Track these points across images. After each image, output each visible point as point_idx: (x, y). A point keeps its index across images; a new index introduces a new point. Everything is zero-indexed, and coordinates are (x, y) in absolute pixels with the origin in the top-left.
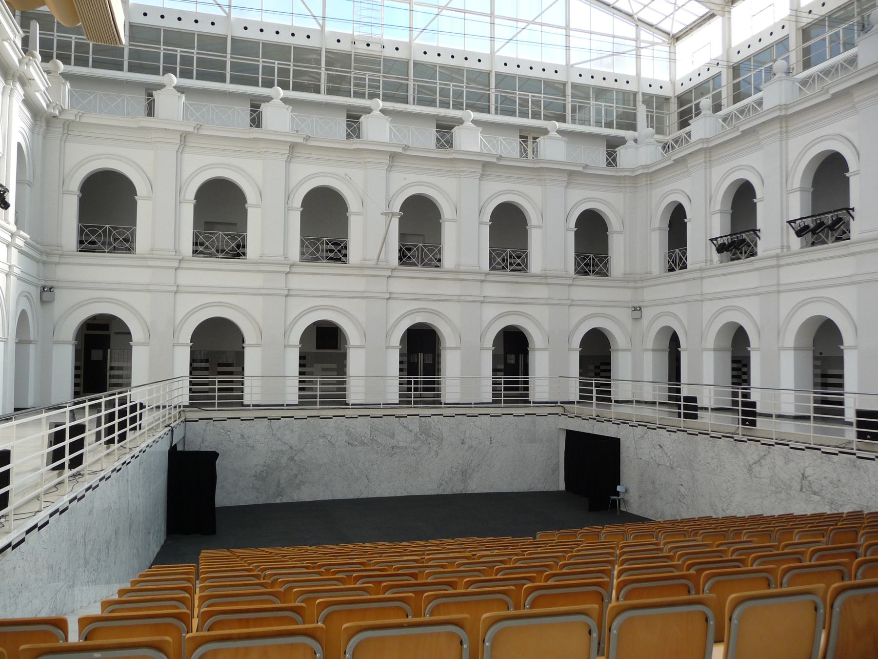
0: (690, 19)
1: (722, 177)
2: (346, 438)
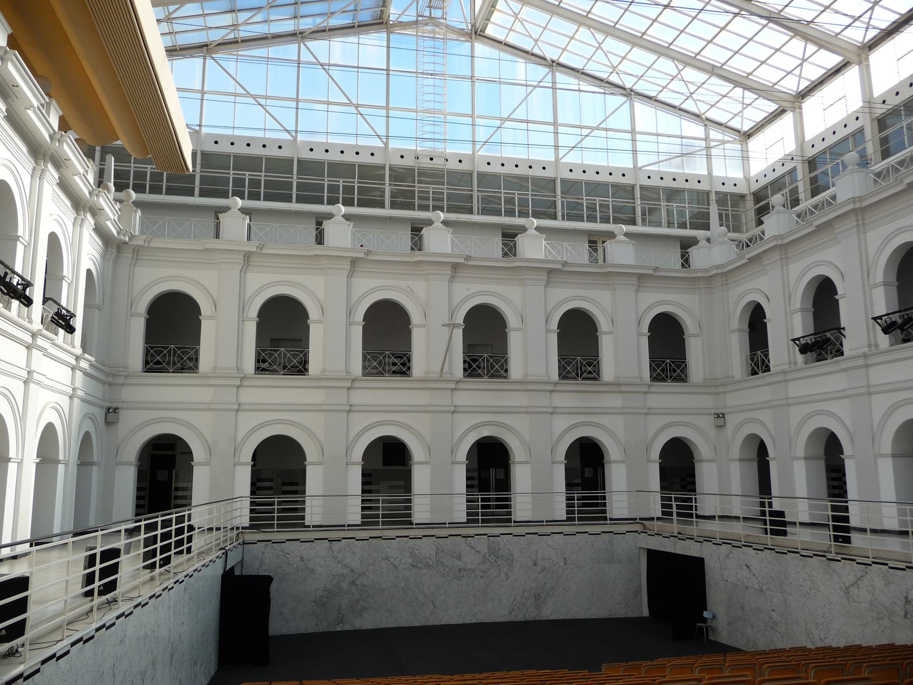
0: (760, 116)
1: (801, 273)
2: (410, 560)
